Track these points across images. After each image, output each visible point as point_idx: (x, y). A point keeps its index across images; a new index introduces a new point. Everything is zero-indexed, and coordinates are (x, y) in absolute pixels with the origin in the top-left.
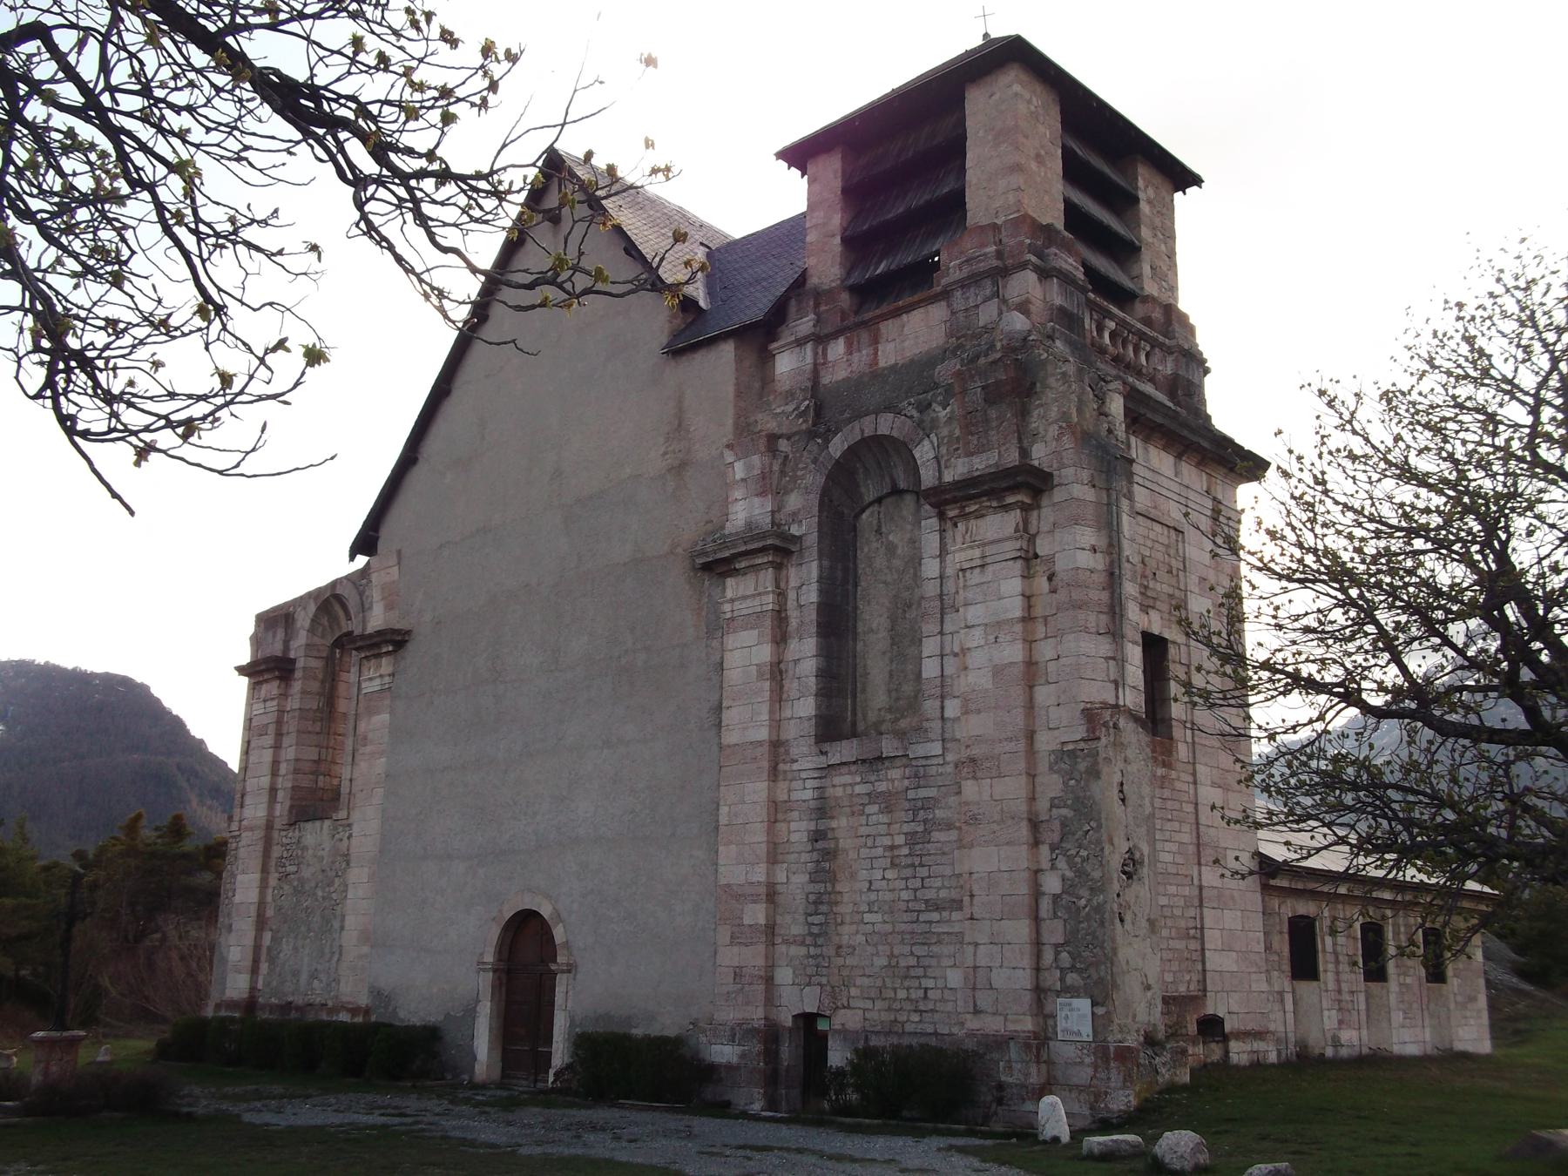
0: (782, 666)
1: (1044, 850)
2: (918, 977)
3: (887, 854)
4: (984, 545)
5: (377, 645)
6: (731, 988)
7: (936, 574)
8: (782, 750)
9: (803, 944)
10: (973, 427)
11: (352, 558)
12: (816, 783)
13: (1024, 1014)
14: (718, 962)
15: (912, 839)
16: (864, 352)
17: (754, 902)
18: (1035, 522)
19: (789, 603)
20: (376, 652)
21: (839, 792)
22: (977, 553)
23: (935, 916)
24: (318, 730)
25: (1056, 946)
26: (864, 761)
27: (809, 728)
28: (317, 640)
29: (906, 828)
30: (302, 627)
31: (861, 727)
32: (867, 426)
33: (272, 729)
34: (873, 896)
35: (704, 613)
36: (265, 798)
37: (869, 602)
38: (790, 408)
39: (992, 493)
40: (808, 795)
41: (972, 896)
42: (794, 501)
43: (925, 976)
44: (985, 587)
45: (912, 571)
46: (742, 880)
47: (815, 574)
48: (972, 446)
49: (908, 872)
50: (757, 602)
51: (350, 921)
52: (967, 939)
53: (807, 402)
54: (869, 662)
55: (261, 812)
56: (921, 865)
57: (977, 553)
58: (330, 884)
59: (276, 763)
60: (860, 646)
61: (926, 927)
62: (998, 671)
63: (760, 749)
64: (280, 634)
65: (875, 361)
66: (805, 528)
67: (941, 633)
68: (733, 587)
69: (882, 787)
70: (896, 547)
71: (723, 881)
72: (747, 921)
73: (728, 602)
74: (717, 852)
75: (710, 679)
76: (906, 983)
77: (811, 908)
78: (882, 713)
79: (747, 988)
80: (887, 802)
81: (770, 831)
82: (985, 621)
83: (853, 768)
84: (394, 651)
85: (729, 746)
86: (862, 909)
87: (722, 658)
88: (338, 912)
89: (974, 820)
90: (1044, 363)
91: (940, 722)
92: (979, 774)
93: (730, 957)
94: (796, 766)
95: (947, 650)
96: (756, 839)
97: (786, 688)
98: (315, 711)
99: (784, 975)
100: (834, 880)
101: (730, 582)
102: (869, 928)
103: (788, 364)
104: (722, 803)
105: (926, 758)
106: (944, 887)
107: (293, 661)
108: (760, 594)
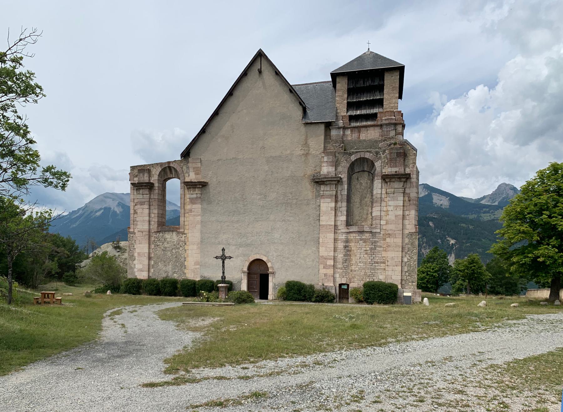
1: (404, 253)
6: (324, 278)
9: (342, 269)
10: (391, 161)
12: (346, 235)
14: (320, 272)
17: (329, 260)
20: (195, 187)
21: (352, 238)
22: (393, 190)
23: (377, 265)
29: (369, 246)
30: (155, 174)
34: (361, 260)
35: (315, 192)
37: (355, 195)
38: (337, 145)
39: (400, 178)
40: (344, 238)
41: (388, 261)
42: (340, 169)
49: (370, 256)
50: (331, 192)
52: (386, 270)
55: (146, 227)
56: (373, 254)
57: (393, 190)
58: (179, 248)
60: (352, 205)
62: (396, 216)
65: (359, 138)
66: (344, 176)
67: (381, 206)
68: (323, 188)
69: (364, 237)
70: (362, 184)
71: (321, 255)
72: (328, 264)
75: (316, 209)
76: (369, 278)
80: (365, 241)
84: (202, 188)
91: (380, 225)
92: (390, 237)
93: (323, 271)
94: (340, 231)
95: (382, 210)
96: (330, 246)
97: (337, 213)
99: (337, 275)
100: (350, 256)
101: (322, 186)
104: (320, 238)
105: (376, 232)
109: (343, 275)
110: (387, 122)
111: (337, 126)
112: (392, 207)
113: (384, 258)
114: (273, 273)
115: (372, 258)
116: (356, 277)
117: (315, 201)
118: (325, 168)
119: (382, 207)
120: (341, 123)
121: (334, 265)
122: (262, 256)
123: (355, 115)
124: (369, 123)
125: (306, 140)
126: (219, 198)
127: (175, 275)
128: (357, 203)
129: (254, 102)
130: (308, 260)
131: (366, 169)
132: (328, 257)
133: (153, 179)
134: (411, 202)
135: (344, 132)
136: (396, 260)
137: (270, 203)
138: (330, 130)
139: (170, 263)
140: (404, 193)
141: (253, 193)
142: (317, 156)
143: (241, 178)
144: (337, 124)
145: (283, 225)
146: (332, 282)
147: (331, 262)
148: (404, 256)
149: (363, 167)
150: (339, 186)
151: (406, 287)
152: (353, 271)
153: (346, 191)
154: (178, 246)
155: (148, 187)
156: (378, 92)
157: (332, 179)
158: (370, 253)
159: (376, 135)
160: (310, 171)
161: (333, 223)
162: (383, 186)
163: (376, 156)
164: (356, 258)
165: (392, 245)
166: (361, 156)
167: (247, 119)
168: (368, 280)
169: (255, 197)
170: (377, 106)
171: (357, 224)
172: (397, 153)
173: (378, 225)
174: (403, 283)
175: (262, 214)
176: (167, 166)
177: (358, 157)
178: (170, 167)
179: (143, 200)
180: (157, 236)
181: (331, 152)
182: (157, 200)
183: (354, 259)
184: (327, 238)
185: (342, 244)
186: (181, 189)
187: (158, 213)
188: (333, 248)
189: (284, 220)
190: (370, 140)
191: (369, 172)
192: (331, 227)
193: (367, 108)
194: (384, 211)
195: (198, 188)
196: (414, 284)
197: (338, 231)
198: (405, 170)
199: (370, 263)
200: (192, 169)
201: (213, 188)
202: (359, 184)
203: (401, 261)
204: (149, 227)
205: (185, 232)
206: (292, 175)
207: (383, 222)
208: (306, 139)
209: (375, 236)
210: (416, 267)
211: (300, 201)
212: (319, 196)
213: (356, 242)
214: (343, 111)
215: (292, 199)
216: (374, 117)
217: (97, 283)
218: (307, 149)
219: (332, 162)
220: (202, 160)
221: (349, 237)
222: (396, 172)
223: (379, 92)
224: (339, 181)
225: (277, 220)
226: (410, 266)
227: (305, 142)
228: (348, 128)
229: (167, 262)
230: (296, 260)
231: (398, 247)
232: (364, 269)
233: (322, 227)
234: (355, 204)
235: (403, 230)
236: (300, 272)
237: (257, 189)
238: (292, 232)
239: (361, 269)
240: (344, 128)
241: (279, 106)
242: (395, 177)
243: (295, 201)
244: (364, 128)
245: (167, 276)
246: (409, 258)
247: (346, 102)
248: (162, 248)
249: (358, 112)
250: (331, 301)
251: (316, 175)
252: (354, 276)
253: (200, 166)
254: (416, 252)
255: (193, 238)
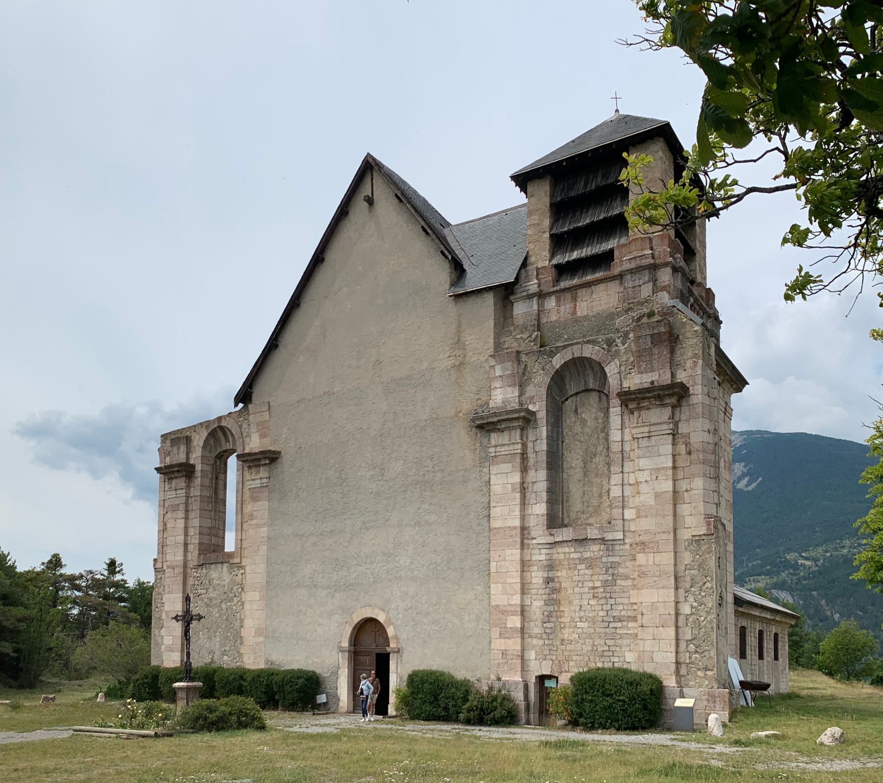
0: (525, 485)
2: (609, 656)
3: (590, 591)
4: (651, 425)
5: (259, 460)
6: (501, 661)
7: (619, 439)
8: (526, 532)
9: (541, 638)
10: (642, 358)
11: (236, 405)
12: (548, 551)
13: (671, 675)
15: (605, 584)
16: (568, 306)
17: (513, 615)
18: (678, 414)
19: (529, 449)
21: (562, 556)
22: (646, 429)
23: (619, 625)
24: (210, 509)
25: (687, 641)
26: (576, 540)
27: (544, 520)
28: (207, 454)
29: (601, 577)
30: (198, 445)
31: (566, 522)
32: (576, 352)
33: (182, 507)
34: (582, 614)
35: (478, 452)
36: (182, 550)
38: (525, 336)
39: (659, 397)
40: (543, 557)
41: (642, 614)
42: (530, 390)
43: (613, 656)
44: (650, 448)
45: (596, 435)
46: (506, 603)
47: (544, 434)
48: (642, 368)
49: (603, 601)
50: (511, 447)
51: (248, 623)
52: (639, 637)
53: (536, 333)
54: (571, 485)
55: (180, 558)
56: (611, 598)
58: (231, 600)
59: (186, 528)
60: (565, 476)
61: (613, 630)
62: (657, 495)
63: (515, 531)
64: (183, 448)
65: (574, 313)
66: (539, 407)
67: (622, 472)
68: (495, 438)
69: (587, 555)
70: (586, 421)
71: (493, 603)
72: (509, 625)
73: (493, 447)
74: (490, 587)
75: (482, 490)
76: (602, 660)
77: (546, 619)
78: (579, 514)
79: (510, 661)
80: (590, 564)
81: (522, 577)
82: (651, 467)
83: (570, 544)
84: (270, 464)
85: (495, 528)
86: (576, 620)
87: (490, 478)
88: (238, 617)
89: (642, 575)
90: (684, 324)
91: (622, 521)
92: (646, 550)
93: (499, 644)
94: (534, 541)
95: (626, 482)
96: (513, 581)
97: (527, 498)
98: (209, 497)
99: (531, 655)
100: (558, 602)
102: (580, 630)
103: (521, 309)
105: (614, 540)
106: (624, 609)
107: (193, 466)
108: (513, 444)
109: (545, 653)
110: (633, 265)
111: (525, 294)
112: (647, 473)
113: (635, 607)
114: (398, 652)
115: (609, 607)
116: (574, 658)
117: (480, 471)
118: (498, 391)
119: (626, 475)
120: (533, 286)
121: (522, 629)
122: (376, 610)
123: (568, 262)
124: (599, 275)
125: (459, 331)
126: (299, 484)
127: (225, 658)
128: (577, 471)
129: (360, 268)
130: (467, 618)
131: (591, 386)
132: (509, 608)
133: (194, 456)
134: (694, 456)
135: (541, 306)
136: (662, 610)
137: (391, 484)
138: (513, 304)
139: (218, 633)
140: (674, 434)
141: (360, 466)
142: (481, 367)
143: (339, 434)
144: (525, 289)
145: (416, 534)
146: (519, 673)
147: (515, 622)
148: (682, 599)
149: (585, 381)
150: (530, 431)
151: (692, 683)
152: (566, 642)
153: (545, 441)
154: (231, 595)
155: (184, 473)
156: (619, 199)
157: (510, 416)
158: (604, 595)
159: (612, 300)
160: (467, 405)
161: (517, 523)
162: (626, 421)
163: (609, 351)
164: (573, 608)
165: (651, 573)
166: (573, 354)
167: (349, 306)
168: (600, 665)
169: (363, 474)
170: (618, 232)
171: (579, 523)
172: (651, 335)
173: (618, 522)
174: (683, 671)
175: (376, 512)
176: (216, 425)
177: (569, 357)
178: (222, 428)
179: (177, 502)
180: (199, 575)
181: (507, 353)
182: (198, 499)
183: (568, 613)
184: (505, 560)
185: (540, 574)
186: (238, 470)
187: (200, 527)
188: (519, 585)
189: (418, 523)
190: (597, 316)
191: (599, 391)
192: (514, 532)
193: (595, 241)
194: (631, 485)
195: (264, 465)
196: (709, 673)
197: (529, 542)
198: (673, 375)
199: (603, 621)
200: (255, 427)
201: (289, 463)
202: (578, 423)
203: (673, 612)
204: (185, 556)
205: (243, 564)
206: (434, 415)
207: (629, 514)
208: (458, 331)
209: (612, 550)
210: (712, 628)
211: (450, 475)
212: (487, 460)
213: (570, 569)
214: (542, 258)
215: (434, 472)
216: (607, 258)
217: (103, 677)
218: (458, 352)
219: (513, 375)
220: (271, 404)
221: (555, 556)
222: (652, 382)
223: (621, 201)
224: (527, 420)
225: (404, 523)
226: (697, 625)
227: (457, 338)
228: (549, 294)
229: (212, 631)
230: (444, 618)
231: (664, 577)
232: (590, 636)
233: (495, 535)
234: (572, 472)
235: (678, 532)
236: (452, 648)
237: (367, 455)
238: (435, 551)
239: (584, 636)
240: (541, 296)
241: (405, 268)
242: (647, 395)
243: (439, 475)
244: (584, 290)
245: (212, 661)
246: (695, 604)
247: (547, 235)
248: (206, 600)
249: (575, 255)
250: (510, 718)
251: (480, 411)
252: (569, 656)
253: (267, 418)
254: (712, 587)
255: (254, 575)
